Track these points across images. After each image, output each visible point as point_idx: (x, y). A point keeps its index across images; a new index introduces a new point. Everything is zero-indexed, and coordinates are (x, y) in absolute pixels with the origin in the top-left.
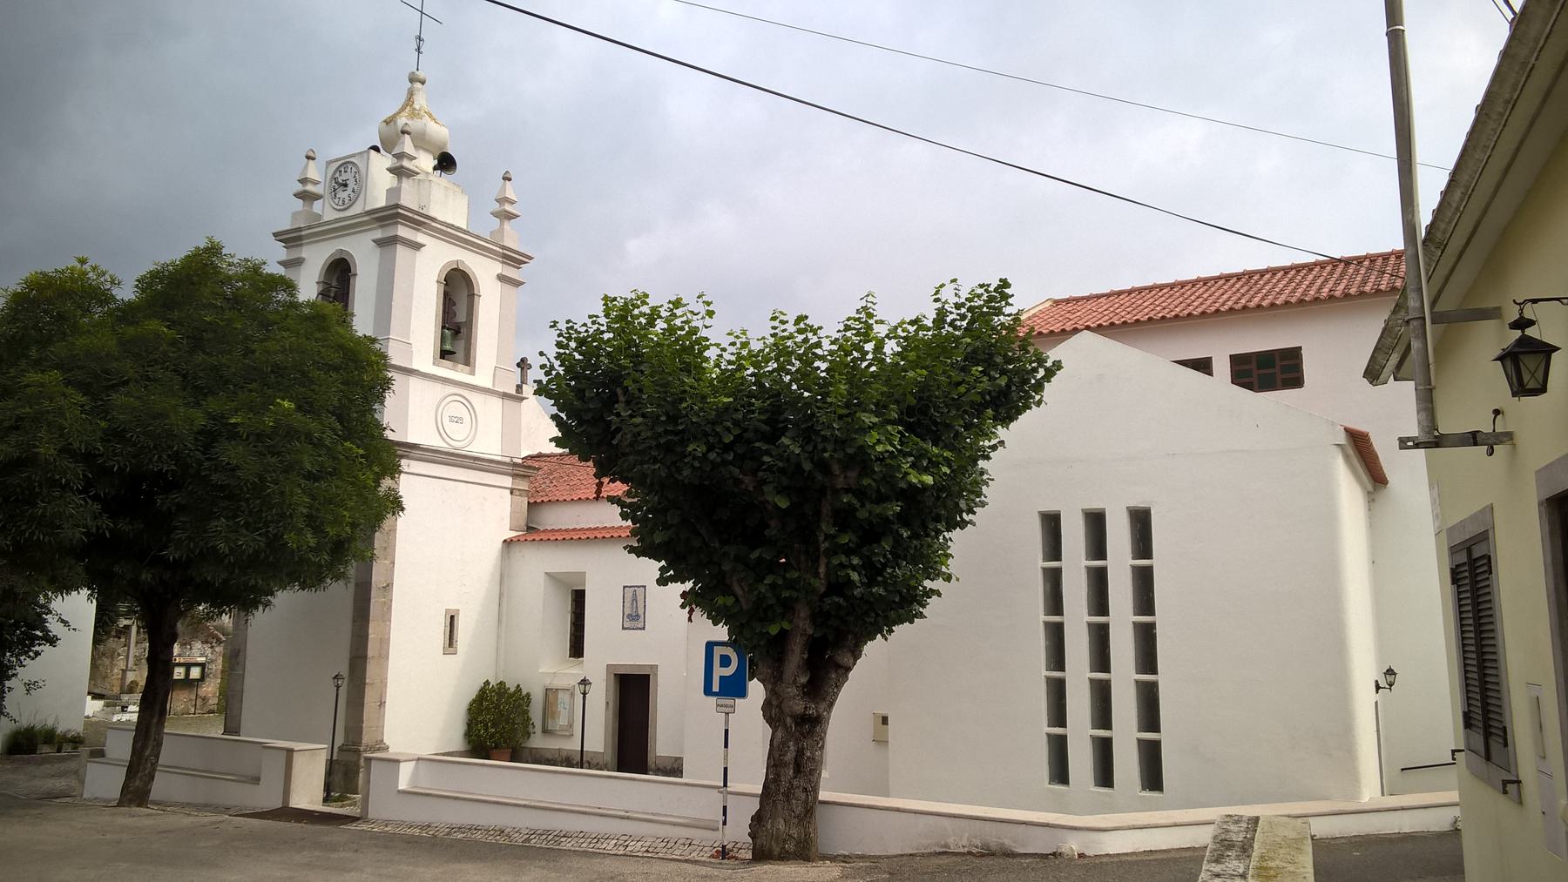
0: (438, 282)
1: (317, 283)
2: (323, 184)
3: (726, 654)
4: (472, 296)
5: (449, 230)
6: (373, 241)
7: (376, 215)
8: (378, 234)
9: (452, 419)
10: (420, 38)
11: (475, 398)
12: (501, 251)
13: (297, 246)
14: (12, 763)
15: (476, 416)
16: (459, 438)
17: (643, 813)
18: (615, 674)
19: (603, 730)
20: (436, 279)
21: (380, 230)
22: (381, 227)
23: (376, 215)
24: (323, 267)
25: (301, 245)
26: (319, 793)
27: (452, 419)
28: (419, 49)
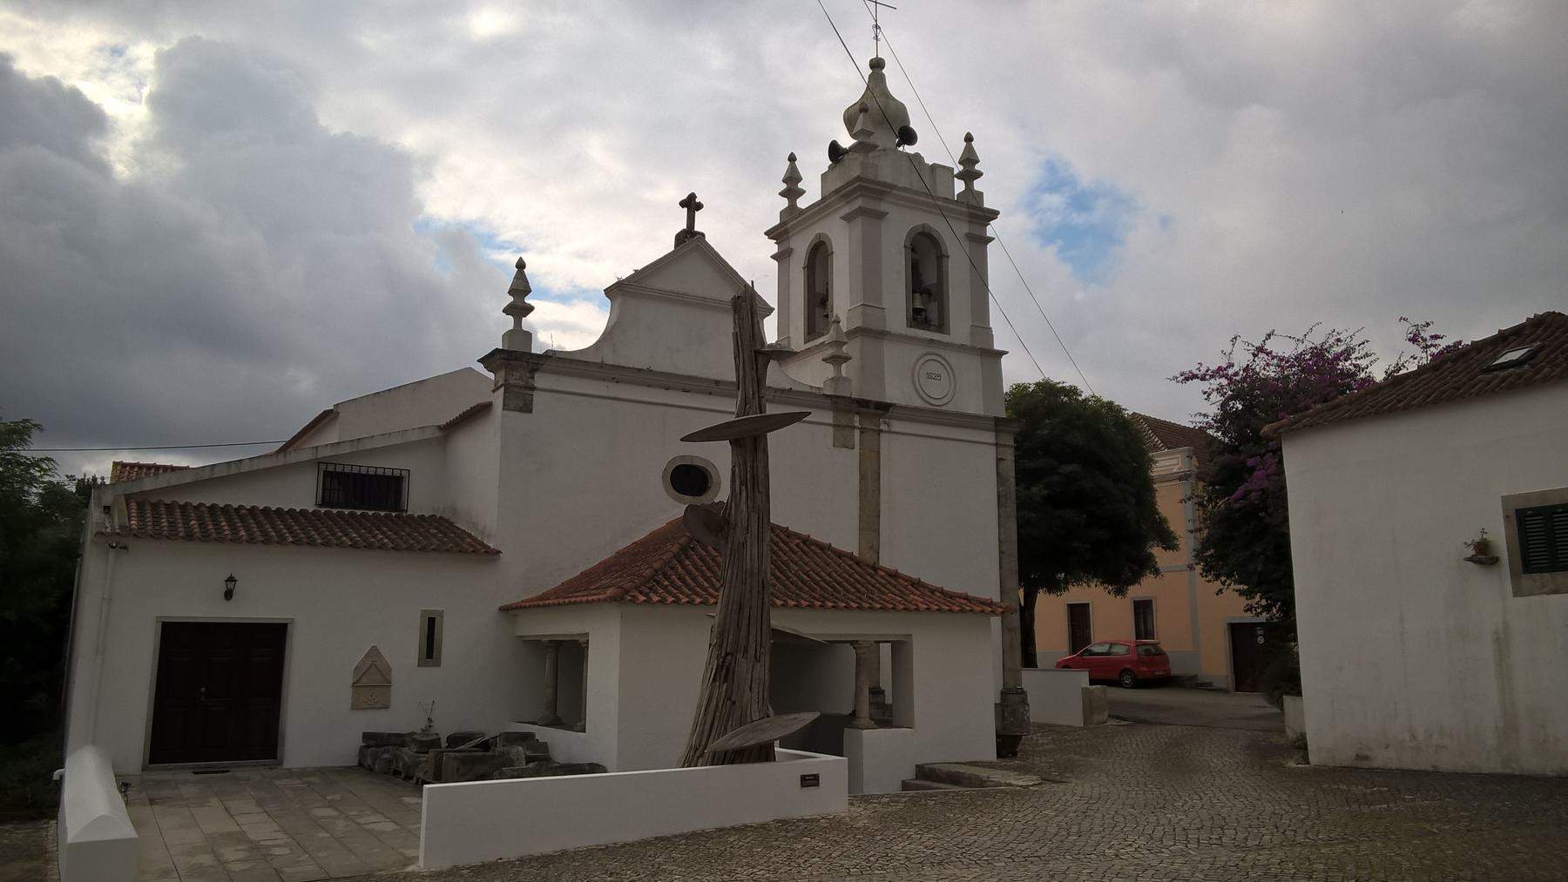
4: (941, 257)
9: (929, 376)
12: (966, 210)
27: (929, 376)
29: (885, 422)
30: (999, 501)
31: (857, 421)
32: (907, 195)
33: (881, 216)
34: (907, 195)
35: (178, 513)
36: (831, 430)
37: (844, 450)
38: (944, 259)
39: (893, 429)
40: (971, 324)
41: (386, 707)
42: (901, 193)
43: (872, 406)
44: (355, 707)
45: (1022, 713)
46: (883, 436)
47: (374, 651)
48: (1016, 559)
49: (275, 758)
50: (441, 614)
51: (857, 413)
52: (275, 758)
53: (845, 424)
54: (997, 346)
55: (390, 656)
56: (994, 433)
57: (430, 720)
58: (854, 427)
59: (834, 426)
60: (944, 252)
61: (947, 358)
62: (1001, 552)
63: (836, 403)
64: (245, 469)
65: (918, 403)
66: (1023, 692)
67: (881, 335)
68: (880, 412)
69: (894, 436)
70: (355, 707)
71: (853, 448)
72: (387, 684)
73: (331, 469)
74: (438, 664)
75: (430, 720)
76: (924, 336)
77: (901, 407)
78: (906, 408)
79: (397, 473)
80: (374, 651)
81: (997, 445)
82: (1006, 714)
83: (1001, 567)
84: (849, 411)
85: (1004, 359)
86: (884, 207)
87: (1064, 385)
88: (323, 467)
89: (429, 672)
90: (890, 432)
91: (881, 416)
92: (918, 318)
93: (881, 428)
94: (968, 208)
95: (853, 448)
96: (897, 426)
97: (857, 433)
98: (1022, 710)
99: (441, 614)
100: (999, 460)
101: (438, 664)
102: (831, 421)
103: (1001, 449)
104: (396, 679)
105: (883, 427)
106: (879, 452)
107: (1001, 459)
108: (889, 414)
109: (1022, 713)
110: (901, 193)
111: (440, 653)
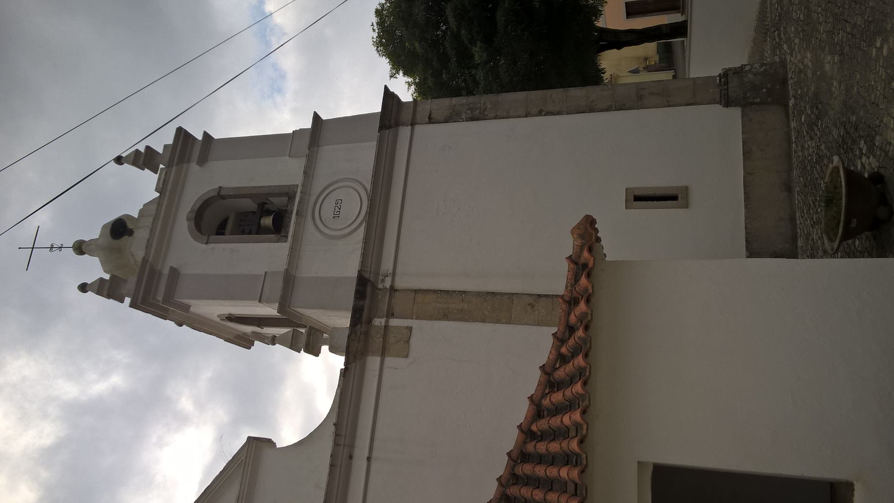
4: (220, 195)
9: (336, 216)
12: (174, 169)
27: (336, 216)
29: (383, 281)
30: (478, 119)
31: (379, 322)
32: (154, 246)
33: (175, 273)
34: (154, 246)
35: (526, 469)
36: (389, 361)
37: (413, 341)
38: (223, 193)
39: (391, 271)
40: (288, 157)
42: (153, 251)
43: (361, 303)
45: (755, 74)
46: (400, 284)
48: (550, 92)
51: (370, 321)
53: (381, 340)
54: (308, 124)
56: (400, 127)
58: (386, 327)
59: (383, 355)
60: (214, 194)
61: (319, 190)
62: (540, 113)
63: (355, 357)
65: (362, 231)
66: (726, 75)
67: (289, 279)
68: (369, 289)
69: (398, 271)
71: (410, 329)
76: (336, 185)
77: (363, 263)
78: (364, 255)
81: (413, 124)
82: (758, 100)
83: (559, 113)
84: (367, 334)
85: (324, 116)
86: (166, 271)
87: (375, 24)
90: (394, 274)
91: (375, 288)
92: (279, 228)
93: (388, 287)
94: (172, 166)
95: (410, 329)
96: (387, 265)
97: (394, 322)
98: (750, 76)
100: (431, 120)
102: (378, 359)
103: (419, 117)
105: (388, 284)
106: (416, 291)
107: (430, 118)
108: (372, 279)
109: (755, 74)
110: (153, 251)
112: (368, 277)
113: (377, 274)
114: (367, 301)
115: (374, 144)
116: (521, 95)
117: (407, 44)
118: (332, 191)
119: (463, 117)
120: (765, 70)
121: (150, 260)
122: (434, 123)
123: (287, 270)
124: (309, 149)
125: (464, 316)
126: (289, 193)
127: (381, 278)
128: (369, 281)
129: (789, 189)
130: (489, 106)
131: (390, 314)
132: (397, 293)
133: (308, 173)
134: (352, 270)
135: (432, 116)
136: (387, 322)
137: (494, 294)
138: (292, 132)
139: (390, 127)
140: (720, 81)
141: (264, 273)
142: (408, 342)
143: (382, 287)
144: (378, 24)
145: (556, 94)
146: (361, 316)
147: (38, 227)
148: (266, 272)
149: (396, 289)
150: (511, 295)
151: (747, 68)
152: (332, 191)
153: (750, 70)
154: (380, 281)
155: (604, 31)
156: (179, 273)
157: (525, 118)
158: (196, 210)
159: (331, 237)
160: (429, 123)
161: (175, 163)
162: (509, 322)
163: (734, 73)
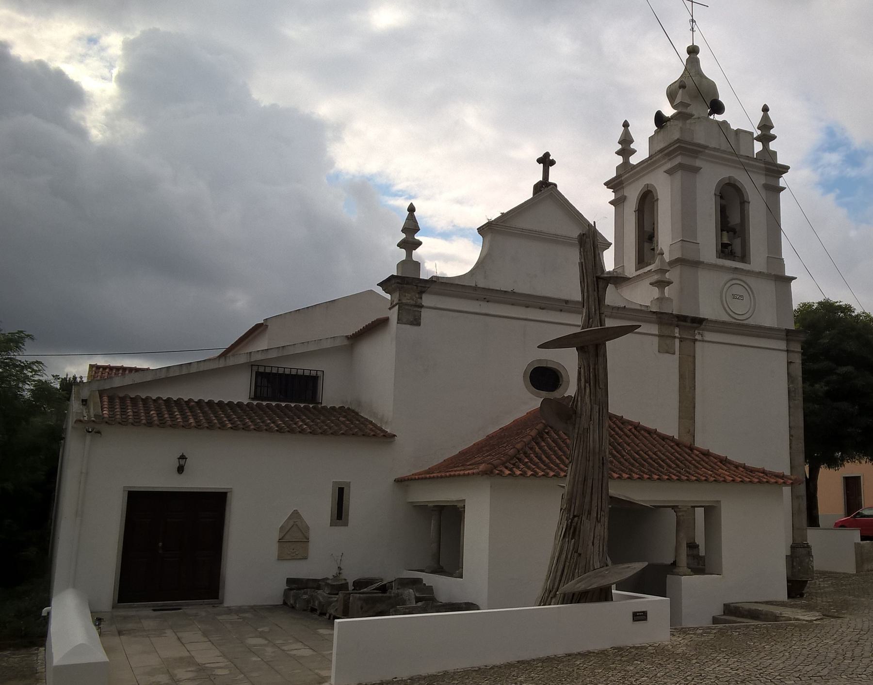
0: (715, 195)
1: (635, 211)
2: (787, 187)
3: (333, 406)
4: (744, 203)
5: (716, 153)
6: (665, 172)
7: (666, 152)
8: (669, 166)
9: (734, 297)
10: (693, 21)
11: (752, 281)
12: (763, 165)
13: (620, 189)
14: (801, 609)
15: (752, 292)
16: (740, 309)
17: (767, 603)
18: (844, 477)
19: (120, 565)
20: (751, 203)
21: (670, 162)
22: (670, 160)
23: (666, 152)
24: (638, 197)
25: (623, 188)
26: (667, 629)
27: (734, 297)
28: (693, 29)
29: (699, 333)
31: (677, 332)
33: (696, 170)
36: (656, 340)
38: (746, 204)
40: (767, 256)
41: (306, 558)
42: (712, 152)
43: (689, 321)
44: (280, 558)
46: (698, 344)
47: (296, 514)
49: (217, 598)
50: (348, 484)
51: (677, 326)
52: (217, 598)
54: (788, 273)
55: (307, 517)
56: (786, 342)
57: (339, 568)
58: (675, 337)
59: (659, 336)
62: (791, 436)
64: (193, 370)
65: (726, 318)
67: (696, 264)
68: (695, 325)
69: (706, 344)
70: (280, 558)
71: (674, 354)
72: (306, 540)
73: (261, 370)
74: (346, 524)
75: (339, 568)
77: (711, 321)
78: (716, 322)
79: (313, 373)
80: (296, 514)
81: (787, 351)
82: (795, 564)
86: (698, 163)
88: (255, 369)
89: (339, 531)
90: (703, 341)
91: (696, 328)
92: (725, 251)
93: (696, 337)
94: (765, 164)
95: (674, 354)
96: (709, 336)
97: (677, 341)
98: (807, 560)
99: (348, 484)
101: (346, 524)
102: (657, 333)
104: (313, 536)
105: (698, 337)
106: (694, 357)
107: (791, 362)
108: (702, 327)
111: (348, 515)
112: (703, 324)
113: (703, 330)
114: (689, 324)
115: (775, 325)
116: (801, 424)
117: (828, 332)
118: (749, 293)
119: (791, 386)
120: (810, 568)
121: (707, 151)
122: (788, 365)
123: (703, 263)
124: (774, 275)
125: (682, 388)
126: (744, 258)
127: (701, 332)
128: (701, 325)
129: (80, 483)
130: (796, 402)
131: (681, 340)
132: (693, 343)
133: (760, 274)
134: (705, 312)
135: (792, 364)
136: (678, 338)
137: (694, 407)
138: (783, 258)
139: (787, 336)
140: (805, 544)
141: (698, 242)
142: (667, 352)
143: (696, 333)
144: (840, 306)
145: (801, 446)
146: (682, 321)
147: (707, 6)
148: (699, 243)
149: (696, 343)
150: (693, 419)
151: (811, 559)
152: (749, 293)
153: (810, 560)
154: (699, 331)
155: (819, 467)
156: (696, 173)
157: (788, 426)
158: (737, 184)
159: (721, 296)
160: (788, 362)
161: (767, 166)
162: (680, 417)
163: (809, 552)
